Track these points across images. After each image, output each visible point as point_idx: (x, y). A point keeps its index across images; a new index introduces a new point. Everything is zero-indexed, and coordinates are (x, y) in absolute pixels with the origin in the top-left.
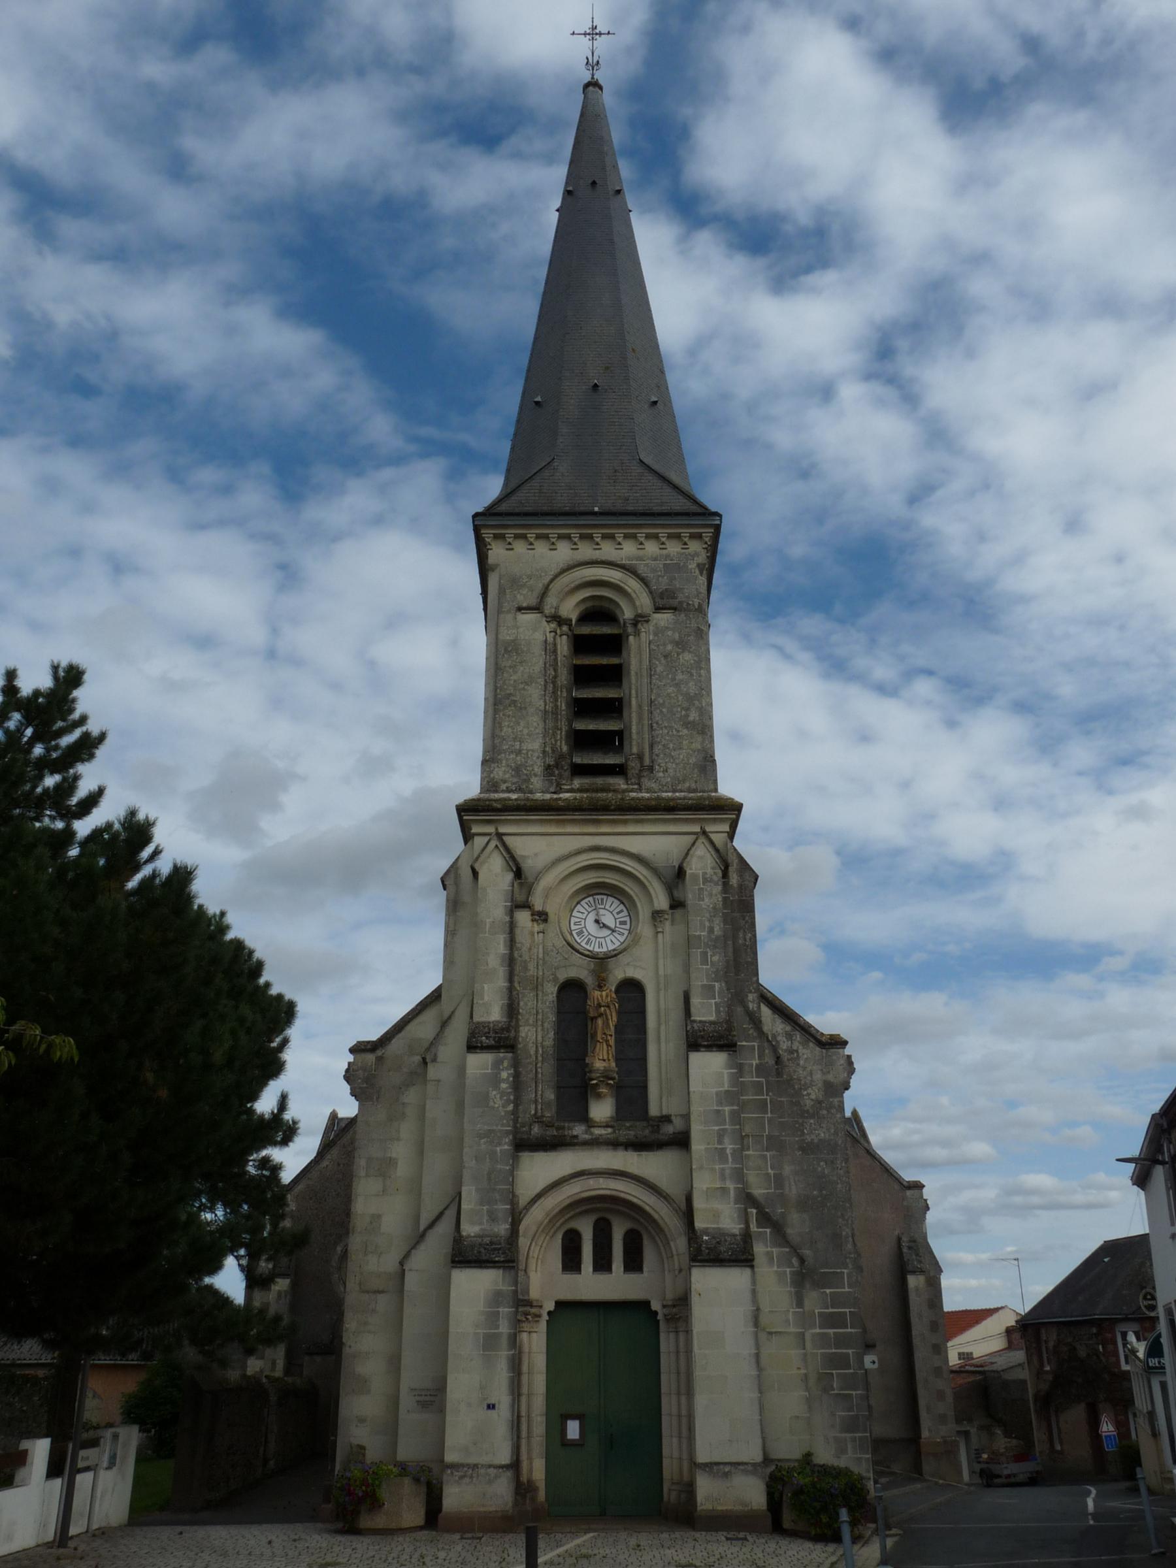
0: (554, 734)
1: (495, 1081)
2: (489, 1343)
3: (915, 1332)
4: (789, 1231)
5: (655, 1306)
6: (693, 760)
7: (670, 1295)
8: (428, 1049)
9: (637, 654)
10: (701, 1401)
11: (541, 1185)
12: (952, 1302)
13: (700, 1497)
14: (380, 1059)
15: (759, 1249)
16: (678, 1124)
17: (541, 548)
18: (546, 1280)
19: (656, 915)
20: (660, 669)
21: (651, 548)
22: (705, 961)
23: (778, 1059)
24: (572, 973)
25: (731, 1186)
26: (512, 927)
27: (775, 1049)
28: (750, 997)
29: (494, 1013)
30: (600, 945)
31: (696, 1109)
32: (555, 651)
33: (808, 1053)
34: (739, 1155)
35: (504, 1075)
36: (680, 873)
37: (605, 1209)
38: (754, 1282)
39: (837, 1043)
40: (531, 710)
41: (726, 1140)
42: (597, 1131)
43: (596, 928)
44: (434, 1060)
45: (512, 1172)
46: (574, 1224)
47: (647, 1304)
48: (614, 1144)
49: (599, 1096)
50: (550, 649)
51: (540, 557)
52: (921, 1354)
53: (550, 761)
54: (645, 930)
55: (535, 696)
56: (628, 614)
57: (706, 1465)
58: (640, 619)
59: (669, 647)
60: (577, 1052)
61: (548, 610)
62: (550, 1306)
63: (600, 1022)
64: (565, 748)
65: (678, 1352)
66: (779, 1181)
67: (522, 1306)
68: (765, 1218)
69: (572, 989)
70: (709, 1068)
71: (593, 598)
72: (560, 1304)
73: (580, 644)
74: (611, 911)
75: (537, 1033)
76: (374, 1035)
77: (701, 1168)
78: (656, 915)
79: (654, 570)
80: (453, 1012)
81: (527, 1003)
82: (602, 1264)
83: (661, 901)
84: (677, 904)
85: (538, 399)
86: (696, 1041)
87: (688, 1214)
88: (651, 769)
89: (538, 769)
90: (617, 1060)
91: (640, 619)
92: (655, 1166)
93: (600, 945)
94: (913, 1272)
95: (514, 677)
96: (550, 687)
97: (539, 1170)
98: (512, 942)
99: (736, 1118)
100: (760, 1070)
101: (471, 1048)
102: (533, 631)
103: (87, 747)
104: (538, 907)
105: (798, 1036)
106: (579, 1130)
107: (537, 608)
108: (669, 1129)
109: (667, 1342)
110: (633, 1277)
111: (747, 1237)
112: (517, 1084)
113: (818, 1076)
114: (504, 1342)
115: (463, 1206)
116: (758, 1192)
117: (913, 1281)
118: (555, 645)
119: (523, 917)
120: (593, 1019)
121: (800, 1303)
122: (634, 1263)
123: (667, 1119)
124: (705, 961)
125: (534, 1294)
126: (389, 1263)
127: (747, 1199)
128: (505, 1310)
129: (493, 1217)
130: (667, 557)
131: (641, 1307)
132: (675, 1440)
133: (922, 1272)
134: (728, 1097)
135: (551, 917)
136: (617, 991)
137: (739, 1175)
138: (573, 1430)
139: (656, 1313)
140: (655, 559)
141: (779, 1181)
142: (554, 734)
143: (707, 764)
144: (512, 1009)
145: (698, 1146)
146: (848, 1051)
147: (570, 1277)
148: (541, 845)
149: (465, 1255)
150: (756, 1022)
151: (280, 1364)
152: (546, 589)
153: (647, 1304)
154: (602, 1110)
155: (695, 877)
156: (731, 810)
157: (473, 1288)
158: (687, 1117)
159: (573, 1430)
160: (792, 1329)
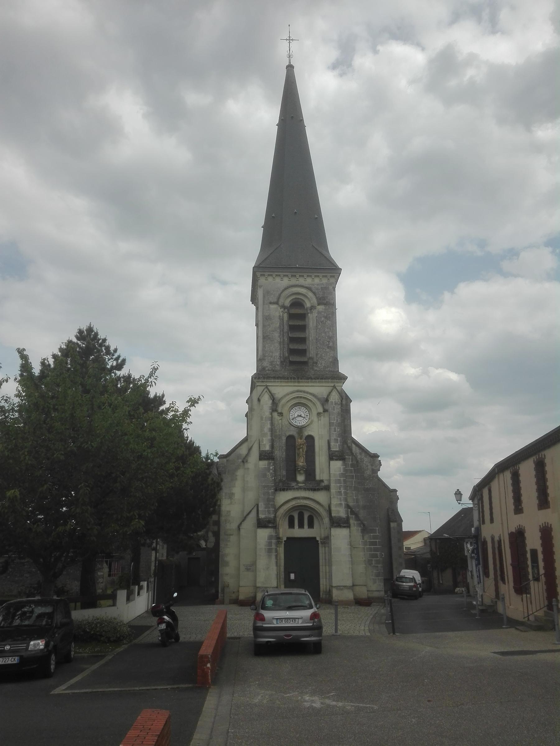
0: (283, 350)
1: (268, 469)
2: (269, 551)
3: (393, 542)
4: (360, 516)
5: (318, 539)
6: (331, 360)
7: (323, 536)
8: (244, 458)
9: (312, 320)
10: (334, 568)
11: (283, 502)
12: (405, 529)
13: (334, 595)
14: (227, 460)
15: (352, 522)
16: (326, 483)
17: (278, 280)
18: (285, 532)
19: (319, 414)
20: (319, 327)
21: (317, 281)
22: (335, 431)
23: (357, 462)
24: (291, 433)
25: (343, 503)
26: (272, 419)
27: (356, 458)
28: (349, 442)
29: (267, 448)
30: (300, 423)
31: (332, 479)
32: (283, 319)
33: (366, 460)
34: (346, 494)
35: (271, 468)
36: (327, 400)
37: (301, 510)
38: (350, 532)
39: (376, 456)
40: (276, 341)
41: (342, 489)
42: (300, 485)
43: (299, 417)
44: (247, 462)
45: (274, 498)
46: (292, 514)
47: (315, 538)
48: (305, 489)
49: (301, 474)
50: (281, 319)
51: (278, 282)
52: (394, 550)
53: (282, 360)
54: (315, 418)
55: (276, 335)
56: (308, 305)
57: (335, 587)
58: (313, 308)
59: (323, 319)
60: (290, 458)
61: (280, 303)
62: (285, 539)
63: (301, 450)
64: (287, 355)
65: (325, 553)
66: (357, 501)
67: (278, 538)
68: (353, 512)
69: (291, 438)
70: (337, 466)
71: (296, 298)
72: (287, 538)
73: (292, 316)
74: (302, 411)
75: (280, 454)
76: (225, 452)
77: (334, 497)
78: (319, 414)
79: (317, 289)
80: (252, 446)
81: (277, 445)
82: (301, 526)
83: (321, 410)
84: (325, 411)
85: (273, 215)
86: (332, 456)
87: (329, 511)
88: (316, 363)
89: (278, 363)
90: (306, 462)
91: (313, 308)
92: (321, 496)
93: (300, 423)
94: (393, 522)
95: (270, 329)
96: (282, 333)
97: (283, 497)
98: (272, 424)
99: (345, 481)
100: (352, 465)
101: (261, 459)
102: (276, 311)
103: (104, 340)
104: (279, 411)
105: (363, 454)
106: (294, 484)
107: (277, 303)
108: (323, 484)
109: (321, 550)
110: (311, 530)
111: (348, 519)
112: (275, 470)
113: (370, 467)
114: (274, 551)
115: (260, 509)
116: (351, 504)
117: (393, 525)
118: (283, 317)
119: (275, 414)
120: (299, 449)
121: (363, 539)
122: (311, 525)
123: (322, 481)
124: (335, 431)
125: (281, 536)
126: (234, 526)
127: (348, 506)
128: (274, 541)
129: (269, 512)
130: (322, 284)
131: (313, 540)
132: (324, 580)
133: (395, 521)
134: (342, 475)
135: (284, 414)
136: (305, 439)
137: (346, 500)
138: (292, 576)
139: (318, 541)
140: (318, 285)
141: (357, 501)
142: (283, 350)
143: (335, 362)
144: (272, 446)
145: (333, 490)
146: (379, 459)
147: (291, 530)
148: (281, 390)
149: (261, 524)
150: (350, 449)
151: (165, 554)
152: (280, 295)
153: (315, 538)
154: (301, 478)
155: (332, 402)
156: (343, 378)
157: (264, 534)
158: (329, 480)
159: (292, 576)
160: (361, 546)
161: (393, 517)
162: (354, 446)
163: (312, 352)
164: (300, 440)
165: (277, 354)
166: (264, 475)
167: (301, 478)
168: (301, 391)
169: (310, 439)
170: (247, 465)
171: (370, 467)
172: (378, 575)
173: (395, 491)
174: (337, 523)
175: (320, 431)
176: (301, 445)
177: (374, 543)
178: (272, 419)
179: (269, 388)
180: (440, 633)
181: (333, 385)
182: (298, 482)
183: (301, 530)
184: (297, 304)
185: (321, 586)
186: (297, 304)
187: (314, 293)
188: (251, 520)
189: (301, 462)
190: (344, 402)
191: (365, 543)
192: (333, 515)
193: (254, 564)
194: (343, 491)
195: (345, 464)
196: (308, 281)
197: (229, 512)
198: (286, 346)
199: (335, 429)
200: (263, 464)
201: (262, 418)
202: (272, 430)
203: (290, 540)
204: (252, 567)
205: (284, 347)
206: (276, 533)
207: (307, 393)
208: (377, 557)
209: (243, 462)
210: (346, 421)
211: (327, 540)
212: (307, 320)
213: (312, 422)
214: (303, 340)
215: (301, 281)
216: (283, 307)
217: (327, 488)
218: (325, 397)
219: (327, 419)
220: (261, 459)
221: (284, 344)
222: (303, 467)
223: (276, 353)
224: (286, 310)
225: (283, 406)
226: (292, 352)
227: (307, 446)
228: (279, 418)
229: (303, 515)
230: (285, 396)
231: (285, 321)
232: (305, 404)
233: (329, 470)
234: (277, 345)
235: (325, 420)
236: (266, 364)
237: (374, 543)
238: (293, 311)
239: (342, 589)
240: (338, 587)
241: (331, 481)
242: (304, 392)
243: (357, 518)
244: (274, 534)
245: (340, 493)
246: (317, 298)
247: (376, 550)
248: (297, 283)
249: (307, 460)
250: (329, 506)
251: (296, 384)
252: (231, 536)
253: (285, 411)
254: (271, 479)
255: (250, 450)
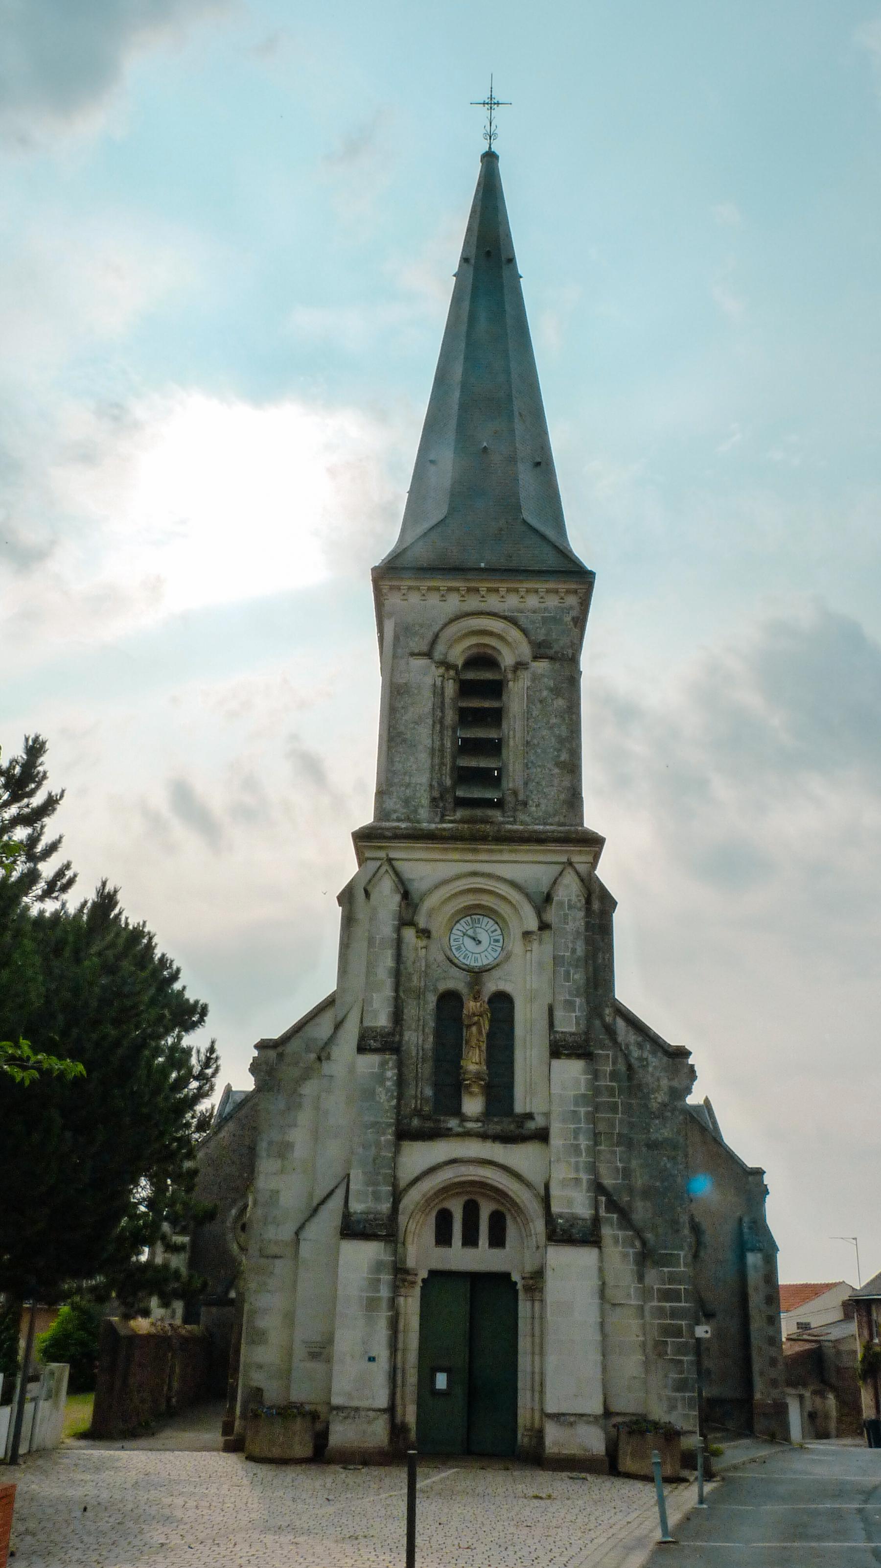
1: (381, 1079)
2: (371, 1305)
5: (515, 1277)
8: (323, 1048)
9: (517, 697)
12: (785, 1277)
15: (607, 1232)
16: (540, 1122)
17: (433, 599)
18: (422, 1252)
20: (535, 713)
21: (532, 601)
23: (630, 1067)
24: (450, 985)
25: (584, 1177)
26: (399, 943)
27: (626, 1057)
29: (382, 1020)
30: (476, 960)
31: (556, 1110)
33: (655, 1061)
36: (548, 898)
37: (473, 1193)
40: (421, 747)
42: (470, 1125)
43: (476, 946)
44: (328, 1058)
47: (507, 1275)
48: (484, 1136)
50: (438, 692)
51: (436, 605)
54: (517, 946)
56: (507, 659)
59: (545, 693)
60: (437, 1047)
61: (437, 655)
62: (424, 1274)
63: (474, 1029)
64: (448, 782)
65: (533, 1318)
66: (627, 1173)
67: (400, 1273)
68: (613, 1205)
69: (449, 1001)
70: (571, 1073)
71: (478, 645)
72: (433, 1273)
73: (466, 689)
74: (486, 929)
75: (418, 1039)
77: (558, 1160)
78: (527, 934)
79: (533, 622)
80: (345, 1017)
81: (411, 1011)
82: (470, 1240)
83: (532, 924)
84: (544, 926)
87: (546, 1200)
88: (525, 804)
89: (425, 801)
92: (522, 1157)
93: (476, 960)
94: (752, 1250)
96: (438, 727)
97: (418, 1157)
98: (399, 957)
99: (592, 1118)
101: (362, 1049)
102: (424, 675)
104: (422, 925)
106: (453, 1123)
107: (428, 654)
108: (531, 1125)
109: (524, 1308)
112: (401, 1082)
114: (384, 1304)
116: (608, 1181)
117: (753, 1259)
118: (443, 688)
119: (409, 934)
120: (469, 1027)
121: (641, 1278)
122: (498, 1240)
123: (530, 1116)
125: (411, 1263)
126: (286, 1232)
127: (598, 1188)
128: (386, 1277)
129: (377, 1197)
130: (546, 609)
135: (434, 934)
136: (490, 1001)
137: (593, 1168)
138: (441, 1381)
139: (516, 1283)
141: (627, 1173)
143: (573, 800)
144: (397, 1016)
145: (556, 1141)
147: (442, 1251)
149: (352, 1229)
150: (610, 1031)
152: (436, 637)
153: (507, 1275)
154: (473, 1105)
155: (561, 904)
156: (593, 843)
157: (361, 1257)
158: (547, 1115)
159: (441, 1381)
161: (753, 1238)
162: (620, 1024)
163: (515, 774)
164: (472, 1004)
165: (423, 779)
166: (369, 1094)
167: (473, 1105)
168: (474, 874)
169: (502, 1003)
170: (327, 1068)
171: (664, 1083)
172: (681, 1386)
173: (759, 1173)
174: (562, 1233)
175: (531, 981)
176: (474, 1015)
177: (667, 1295)
178: (399, 943)
179: (397, 864)
180: (245, 1316)
181: (564, 859)
182: (463, 1118)
183: (470, 1252)
184: (483, 660)
185: (520, 1412)
186: (483, 660)
187: (524, 631)
188: (330, 1218)
189: (474, 1062)
190: (596, 906)
191: (645, 1294)
192: (555, 1209)
193: (329, 1341)
194: (584, 1142)
195: (596, 1075)
196: (512, 602)
197: (275, 1194)
198: (448, 760)
199: (567, 973)
200: (369, 1063)
201: (371, 941)
202: (398, 974)
203: (438, 1278)
204: (321, 1351)
205: (442, 764)
206: (395, 1253)
207: (499, 879)
208: (682, 1337)
209: (319, 1059)
210: (600, 955)
211: (537, 1276)
212: (504, 698)
213: (508, 957)
214: (495, 748)
215: (493, 603)
216: (446, 664)
217: (542, 1136)
218: (545, 890)
219: (548, 948)
220: (362, 1049)
221: (442, 757)
222: (478, 1076)
223: (421, 774)
224: (452, 673)
225: (430, 915)
226: (464, 776)
227: (491, 1021)
228: (421, 943)
229: (476, 1211)
230: (437, 887)
231: (447, 701)
232: (492, 910)
233: (550, 1086)
234: (424, 757)
235: (543, 949)
236: (390, 804)
237: (667, 1295)
238: (470, 675)
239: (571, 1424)
240: (557, 1417)
241: (553, 1116)
242: (489, 876)
243: (625, 1217)
244: (388, 1258)
245: (576, 1149)
246: (530, 642)
247: (674, 1314)
248: (483, 606)
249: (490, 1061)
250: (547, 1187)
251: (470, 857)
252: (277, 1262)
253: (437, 926)
254: (386, 1106)
255: (338, 1026)
